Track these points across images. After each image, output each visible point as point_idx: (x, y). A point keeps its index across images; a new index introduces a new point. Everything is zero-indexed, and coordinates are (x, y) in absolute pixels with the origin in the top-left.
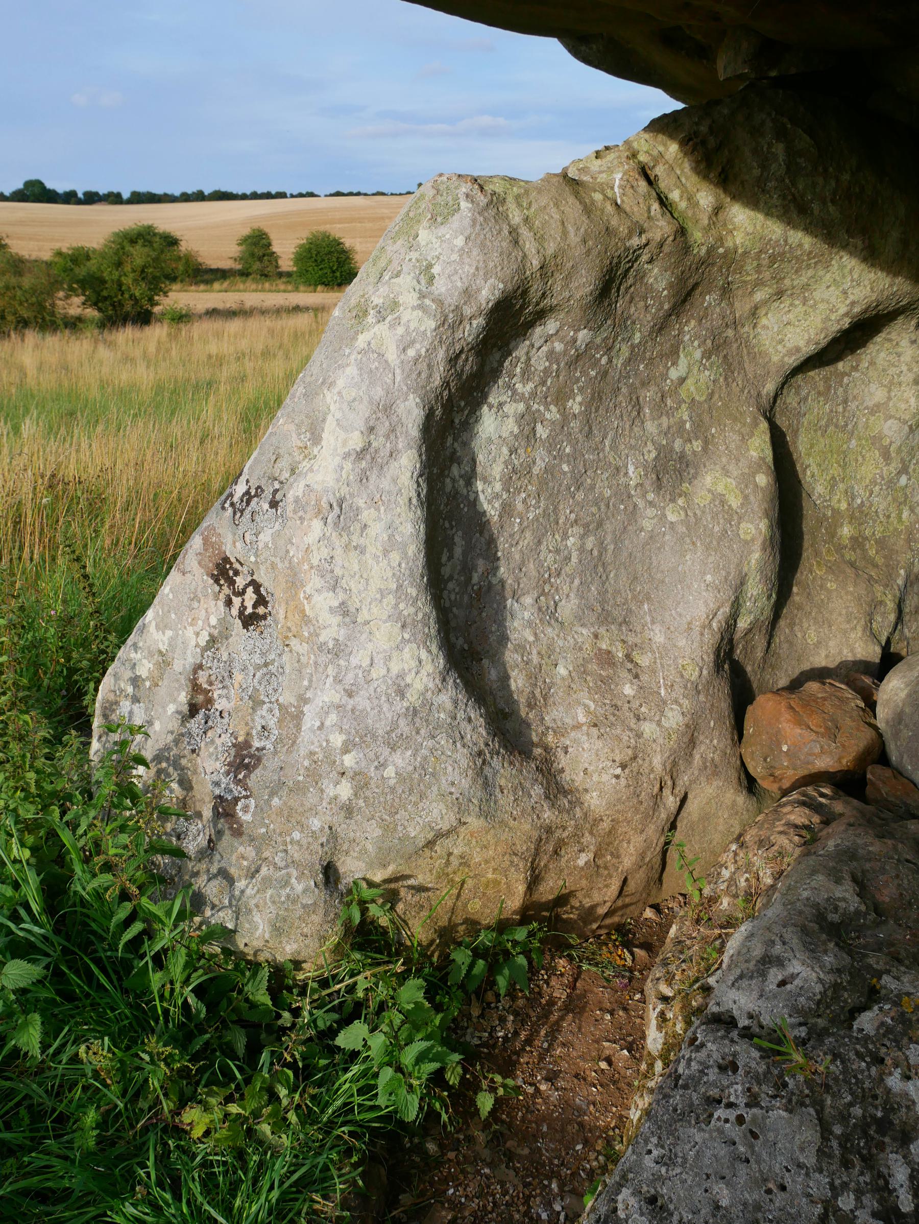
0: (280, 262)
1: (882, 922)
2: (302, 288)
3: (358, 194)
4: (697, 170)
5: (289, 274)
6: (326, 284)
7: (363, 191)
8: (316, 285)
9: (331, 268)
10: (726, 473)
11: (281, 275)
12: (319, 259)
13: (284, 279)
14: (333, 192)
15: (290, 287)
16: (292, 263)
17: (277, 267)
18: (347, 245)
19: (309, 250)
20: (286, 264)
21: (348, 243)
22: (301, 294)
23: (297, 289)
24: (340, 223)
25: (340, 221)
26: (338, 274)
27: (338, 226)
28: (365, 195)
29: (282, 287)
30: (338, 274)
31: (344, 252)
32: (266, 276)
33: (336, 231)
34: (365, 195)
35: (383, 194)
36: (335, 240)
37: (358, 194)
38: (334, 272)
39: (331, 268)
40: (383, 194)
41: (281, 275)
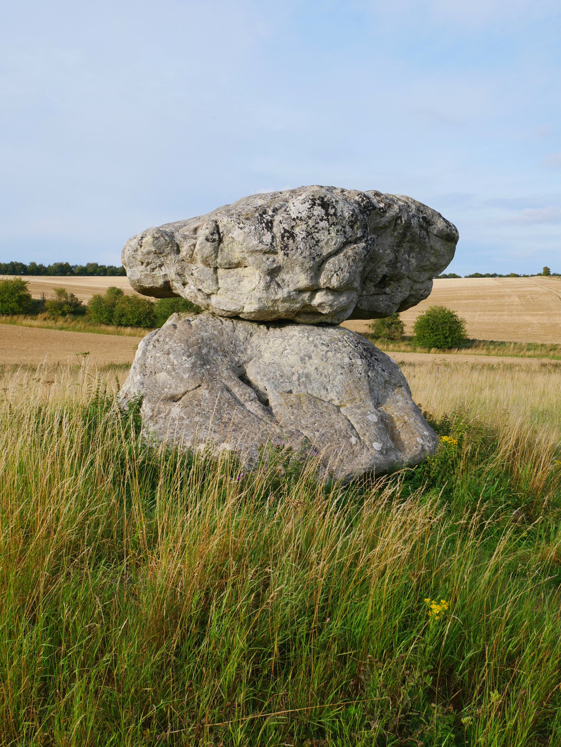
0: (405, 329)
1: (207, 361)
2: (418, 349)
3: (494, 276)
4: (421, 317)
5: (410, 339)
6: (424, 346)
7: (498, 273)
8: (430, 348)
9: (444, 335)
10: (349, 397)
11: (404, 339)
12: (435, 327)
13: (406, 342)
14: (472, 273)
15: (409, 348)
16: (412, 330)
17: (402, 332)
18: (459, 318)
19: (428, 321)
20: (409, 331)
21: (460, 315)
22: (416, 354)
23: (414, 351)
24: (465, 299)
25: (466, 298)
26: (449, 340)
27: (464, 302)
28: (501, 276)
29: (403, 348)
30: (449, 340)
31: (456, 322)
32: (392, 339)
33: (450, 307)
34: (501, 276)
35: (517, 276)
36: (449, 313)
37: (494, 276)
38: (446, 338)
39: (444, 335)
40: (517, 276)
41: (404, 339)
